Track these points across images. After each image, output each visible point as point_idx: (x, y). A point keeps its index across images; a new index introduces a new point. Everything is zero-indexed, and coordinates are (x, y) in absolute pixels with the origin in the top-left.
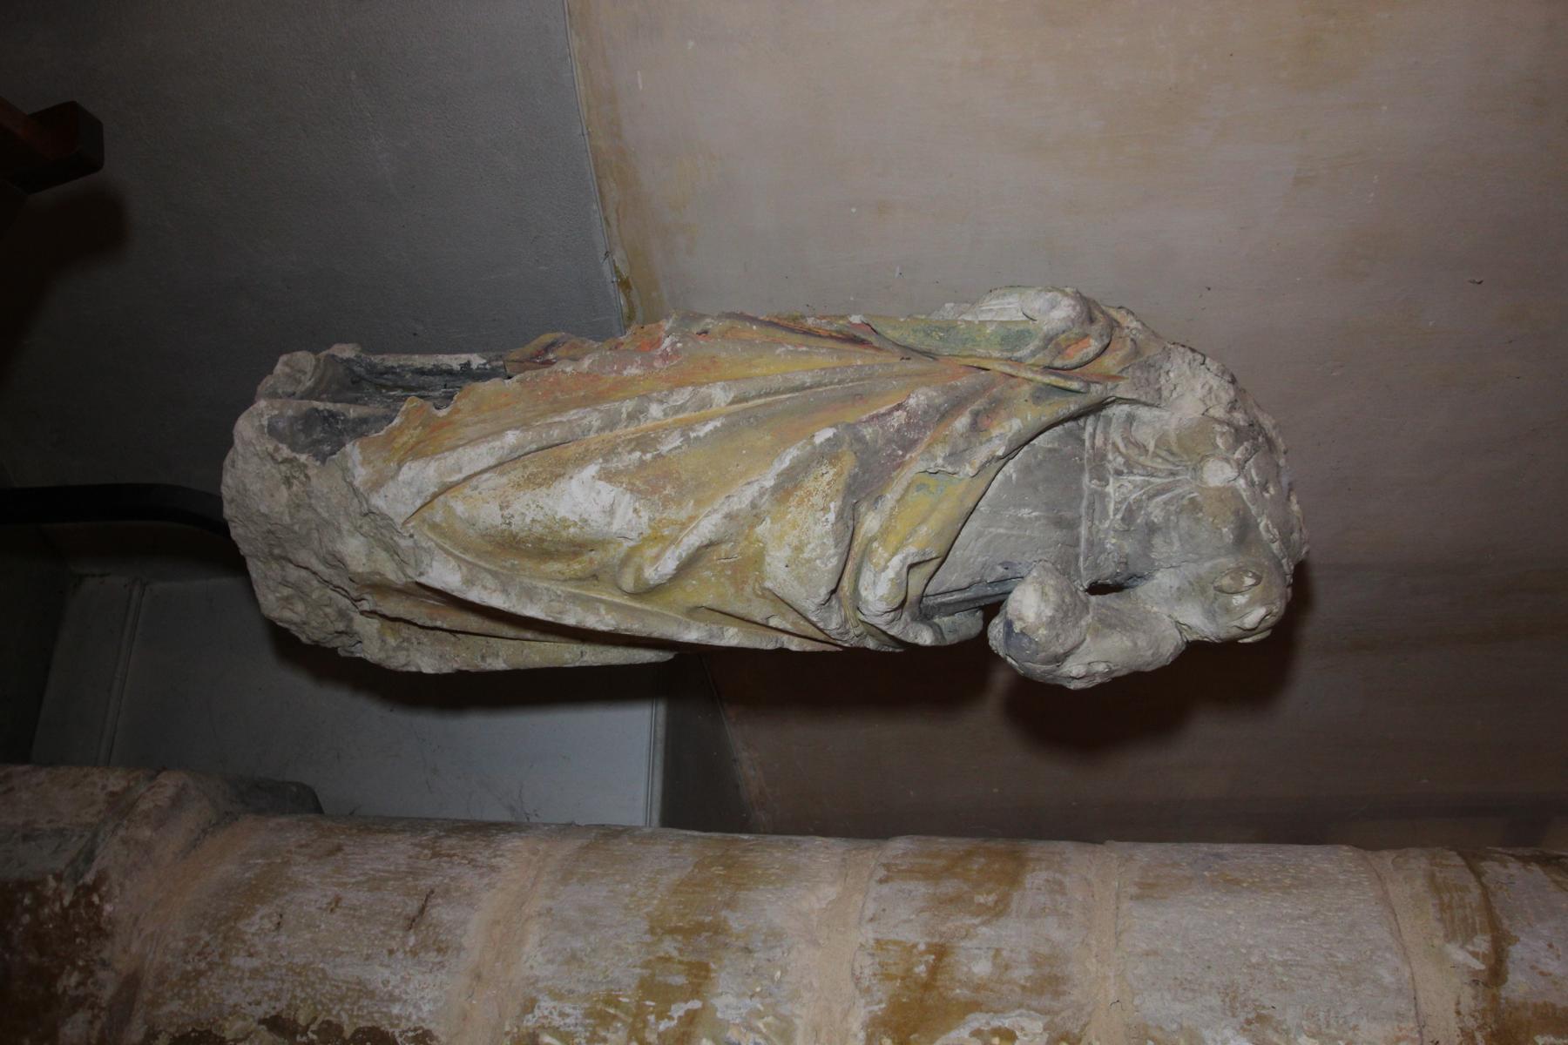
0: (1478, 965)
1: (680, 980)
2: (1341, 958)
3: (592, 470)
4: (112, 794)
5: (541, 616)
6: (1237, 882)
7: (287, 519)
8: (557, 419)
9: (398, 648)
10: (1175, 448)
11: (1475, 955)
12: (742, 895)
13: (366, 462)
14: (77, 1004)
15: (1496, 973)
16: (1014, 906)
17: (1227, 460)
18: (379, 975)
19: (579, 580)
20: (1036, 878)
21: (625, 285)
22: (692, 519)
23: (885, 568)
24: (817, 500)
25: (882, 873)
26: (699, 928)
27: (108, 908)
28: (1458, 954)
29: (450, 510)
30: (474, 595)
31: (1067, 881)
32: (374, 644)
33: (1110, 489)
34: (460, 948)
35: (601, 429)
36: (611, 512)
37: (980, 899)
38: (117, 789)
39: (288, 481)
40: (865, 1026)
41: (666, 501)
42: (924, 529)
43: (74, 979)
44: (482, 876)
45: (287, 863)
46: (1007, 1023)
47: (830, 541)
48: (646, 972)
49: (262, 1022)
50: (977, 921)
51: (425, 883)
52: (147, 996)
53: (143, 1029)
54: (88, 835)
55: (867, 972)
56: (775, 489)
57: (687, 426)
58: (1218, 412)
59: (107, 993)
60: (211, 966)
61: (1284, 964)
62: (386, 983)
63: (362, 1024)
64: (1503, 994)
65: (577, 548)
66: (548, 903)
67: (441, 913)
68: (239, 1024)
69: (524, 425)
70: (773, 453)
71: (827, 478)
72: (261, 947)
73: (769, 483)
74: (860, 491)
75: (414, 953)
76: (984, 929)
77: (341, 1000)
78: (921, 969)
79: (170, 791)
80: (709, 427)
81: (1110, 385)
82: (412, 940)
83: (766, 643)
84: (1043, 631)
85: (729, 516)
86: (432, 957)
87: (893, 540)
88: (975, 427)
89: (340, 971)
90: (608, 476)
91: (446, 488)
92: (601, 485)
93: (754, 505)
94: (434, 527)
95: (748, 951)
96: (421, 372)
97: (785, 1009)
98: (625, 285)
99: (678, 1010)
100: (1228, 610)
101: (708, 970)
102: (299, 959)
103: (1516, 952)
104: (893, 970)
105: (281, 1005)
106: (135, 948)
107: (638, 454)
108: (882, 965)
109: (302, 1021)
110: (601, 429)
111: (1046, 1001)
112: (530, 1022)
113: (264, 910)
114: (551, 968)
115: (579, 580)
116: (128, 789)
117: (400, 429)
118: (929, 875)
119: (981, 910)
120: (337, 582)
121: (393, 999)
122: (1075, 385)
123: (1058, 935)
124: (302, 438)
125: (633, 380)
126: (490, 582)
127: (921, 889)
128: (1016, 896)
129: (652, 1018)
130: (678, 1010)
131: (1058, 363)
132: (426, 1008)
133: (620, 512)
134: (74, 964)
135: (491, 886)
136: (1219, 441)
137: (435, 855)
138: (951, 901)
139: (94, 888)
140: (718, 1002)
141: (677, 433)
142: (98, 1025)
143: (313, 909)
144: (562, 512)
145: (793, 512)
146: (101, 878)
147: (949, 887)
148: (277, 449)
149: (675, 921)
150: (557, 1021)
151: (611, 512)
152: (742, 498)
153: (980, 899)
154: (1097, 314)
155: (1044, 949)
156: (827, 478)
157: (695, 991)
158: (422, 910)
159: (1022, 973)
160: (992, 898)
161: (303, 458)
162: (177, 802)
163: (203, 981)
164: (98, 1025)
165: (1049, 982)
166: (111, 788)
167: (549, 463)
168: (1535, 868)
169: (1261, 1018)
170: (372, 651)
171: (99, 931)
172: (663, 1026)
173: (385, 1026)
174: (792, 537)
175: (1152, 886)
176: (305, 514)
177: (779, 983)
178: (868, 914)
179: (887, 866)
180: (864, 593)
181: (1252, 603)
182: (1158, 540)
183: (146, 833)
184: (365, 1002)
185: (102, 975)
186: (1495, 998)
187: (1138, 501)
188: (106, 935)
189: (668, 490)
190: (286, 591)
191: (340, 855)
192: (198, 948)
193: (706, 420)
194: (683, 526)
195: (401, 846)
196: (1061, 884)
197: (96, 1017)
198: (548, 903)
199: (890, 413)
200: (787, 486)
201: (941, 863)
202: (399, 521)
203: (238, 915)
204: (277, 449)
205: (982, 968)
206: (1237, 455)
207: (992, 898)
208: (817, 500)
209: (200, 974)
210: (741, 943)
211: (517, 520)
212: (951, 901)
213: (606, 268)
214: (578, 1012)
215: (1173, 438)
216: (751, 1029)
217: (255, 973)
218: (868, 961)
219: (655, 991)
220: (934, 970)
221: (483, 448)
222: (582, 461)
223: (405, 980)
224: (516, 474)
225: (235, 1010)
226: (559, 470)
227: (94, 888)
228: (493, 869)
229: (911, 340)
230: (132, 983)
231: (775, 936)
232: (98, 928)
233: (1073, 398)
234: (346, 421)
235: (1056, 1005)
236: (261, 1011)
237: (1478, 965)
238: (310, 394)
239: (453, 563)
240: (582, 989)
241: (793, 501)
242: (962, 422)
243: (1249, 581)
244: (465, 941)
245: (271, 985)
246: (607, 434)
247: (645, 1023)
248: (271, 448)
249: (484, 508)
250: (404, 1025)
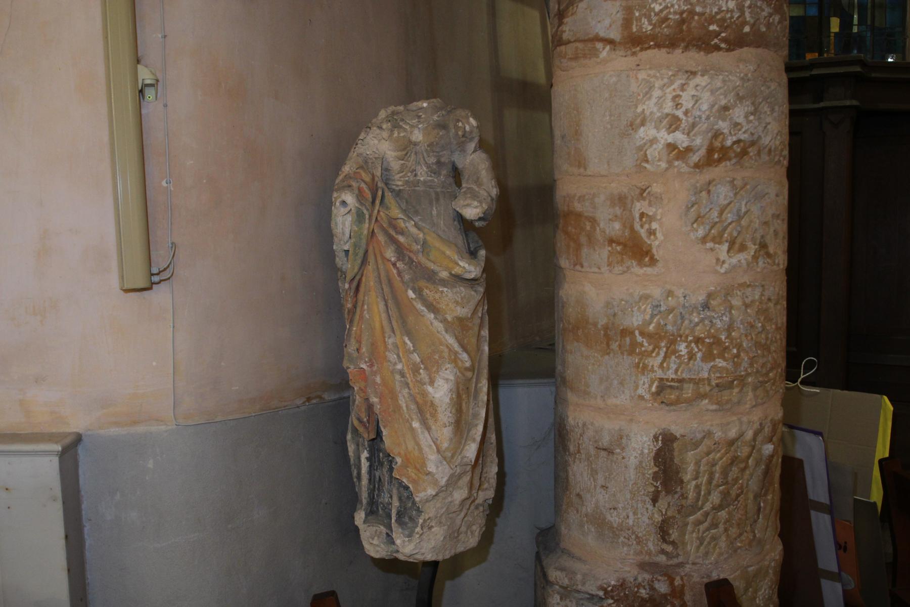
0: (608, 48)
1: (628, 339)
2: (607, 95)
3: (430, 389)
4: (561, 599)
5: (484, 410)
6: (576, 131)
7: (446, 527)
8: (405, 408)
9: (488, 482)
10: (404, 153)
11: (604, 49)
12: (591, 321)
13: (425, 490)
14: (652, 588)
15: (611, 42)
16: (590, 215)
17: (411, 132)
18: (633, 461)
19: (468, 396)
20: (578, 207)
21: (309, 399)
22: (447, 347)
23: (464, 268)
24: (437, 296)
25: (578, 267)
26: (606, 335)
27: (613, 583)
28: (604, 54)
29: (447, 449)
30: (478, 438)
31: (578, 195)
32: (487, 494)
33: (422, 179)
34: (620, 430)
35: (409, 388)
36: (447, 380)
37: (588, 228)
38: (558, 597)
39: (430, 528)
40: (641, 267)
41: (441, 357)
42: (448, 252)
43: (642, 591)
44: (588, 429)
45: (586, 515)
46: (637, 216)
47: (455, 290)
48: (626, 353)
49: (654, 506)
50: (598, 229)
51: (592, 451)
52: (647, 557)
53: (661, 556)
54: (581, 602)
55: (621, 268)
56: (434, 313)
57: (408, 352)
58: (385, 134)
59: (647, 576)
60: (633, 533)
61: (610, 116)
62: (636, 457)
63: (652, 464)
64: (618, 40)
65: (459, 396)
66: (599, 397)
67: (605, 441)
68: (656, 516)
69: (408, 422)
70: (419, 314)
71: (722, 197)
72: (624, 514)
73: (432, 316)
74: (431, 277)
75: (623, 449)
76: (602, 225)
77: (644, 474)
78: (619, 248)
79: (558, 573)
80: (408, 342)
81: (376, 179)
82: (618, 451)
83: (487, 318)
84: (484, 205)
85: (446, 331)
86: (624, 441)
87: (451, 265)
88: (402, 233)
89: (632, 477)
90: (432, 383)
91: (438, 451)
92: (436, 385)
93: (441, 322)
94: (452, 457)
95: (615, 315)
96: (370, 480)
97: (637, 298)
98: (309, 399)
99: (639, 339)
100: (471, 132)
101: (623, 330)
102: (628, 496)
103: (602, 34)
104: (619, 258)
105: (647, 499)
106: (627, 569)
107: (421, 371)
108: (618, 263)
109: (652, 489)
110: (409, 388)
111: (629, 201)
112: (647, 396)
113: (609, 517)
114: (626, 391)
115: (468, 396)
116: (558, 593)
117: (408, 478)
118: (579, 247)
119: (593, 228)
120: (467, 506)
121: (642, 453)
122: (380, 193)
123: (602, 197)
124: (410, 525)
125: (383, 379)
126: (473, 432)
127: (585, 251)
128: (586, 214)
129: (643, 349)
130: (639, 339)
131: (371, 200)
132: (645, 439)
133: (446, 376)
134: (637, 592)
135: (592, 424)
136: (402, 135)
137: (579, 452)
138: (590, 239)
139: (605, 590)
140: (636, 324)
141: (411, 356)
142: (660, 578)
143: (607, 496)
144: (448, 400)
145: (442, 306)
146: (601, 588)
147: (583, 239)
148: (418, 533)
149: (604, 345)
150: (647, 385)
151: (447, 380)
152: (439, 326)
153: (588, 228)
154: (345, 183)
155: (608, 203)
156: (428, 292)
157: (632, 333)
158: (604, 450)
159: (618, 211)
160: (587, 223)
161: (421, 521)
162: (562, 569)
163: (640, 535)
164: (660, 578)
165: (621, 200)
166: (559, 601)
167: (425, 409)
168: (565, 20)
169: (631, 125)
170: (491, 494)
171: (623, 584)
172: (646, 344)
173: (652, 454)
174: (452, 306)
175: (579, 162)
176: (443, 520)
177: (626, 302)
178: (597, 270)
179: (575, 265)
180: (472, 276)
181: (469, 123)
182: (443, 160)
183: (579, 577)
184: (644, 464)
185: (640, 579)
186: (620, 43)
187: (428, 168)
188: (624, 580)
189: (436, 357)
190: (469, 533)
191: (581, 493)
192: (626, 541)
193: (405, 343)
194: (450, 350)
195: (575, 468)
196: (580, 197)
197: (656, 579)
198: (599, 397)
199: (397, 268)
200: (432, 308)
201: (572, 244)
202: (451, 471)
203: (611, 527)
204: (418, 533)
205: (617, 226)
206: (407, 127)
207: (587, 223)
208: (437, 296)
209: (637, 537)
210: (612, 318)
211: (450, 420)
212: (590, 239)
213: (303, 408)
214: (643, 378)
215: (399, 153)
216: (645, 310)
217: (635, 514)
218: (616, 268)
219: (633, 348)
220: (619, 243)
221: (421, 437)
222: (424, 394)
223: (634, 450)
224: (431, 422)
225: (650, 518)
226: (429, 404)
227: (605, 590)
228: (584, 425)
229: (359, 262)
230: (642, 566)
231: (608, 304)
232: (621, 585)
233: (386, 194)
234: (400, 506)
235: (630, 198)
236: (650, 507)
237: (608, 48)
238: (389, 527)
239: (467, 447)
240: (634, 378)
241: (438, 306)
242: (401, 239)
243: (460, 124)
244: (617, 428)
245: (640, 505)
246: (411, 385)
247: (645, 351)
248: (417, 536)
249: (445, 434)
250: (652, 447)
